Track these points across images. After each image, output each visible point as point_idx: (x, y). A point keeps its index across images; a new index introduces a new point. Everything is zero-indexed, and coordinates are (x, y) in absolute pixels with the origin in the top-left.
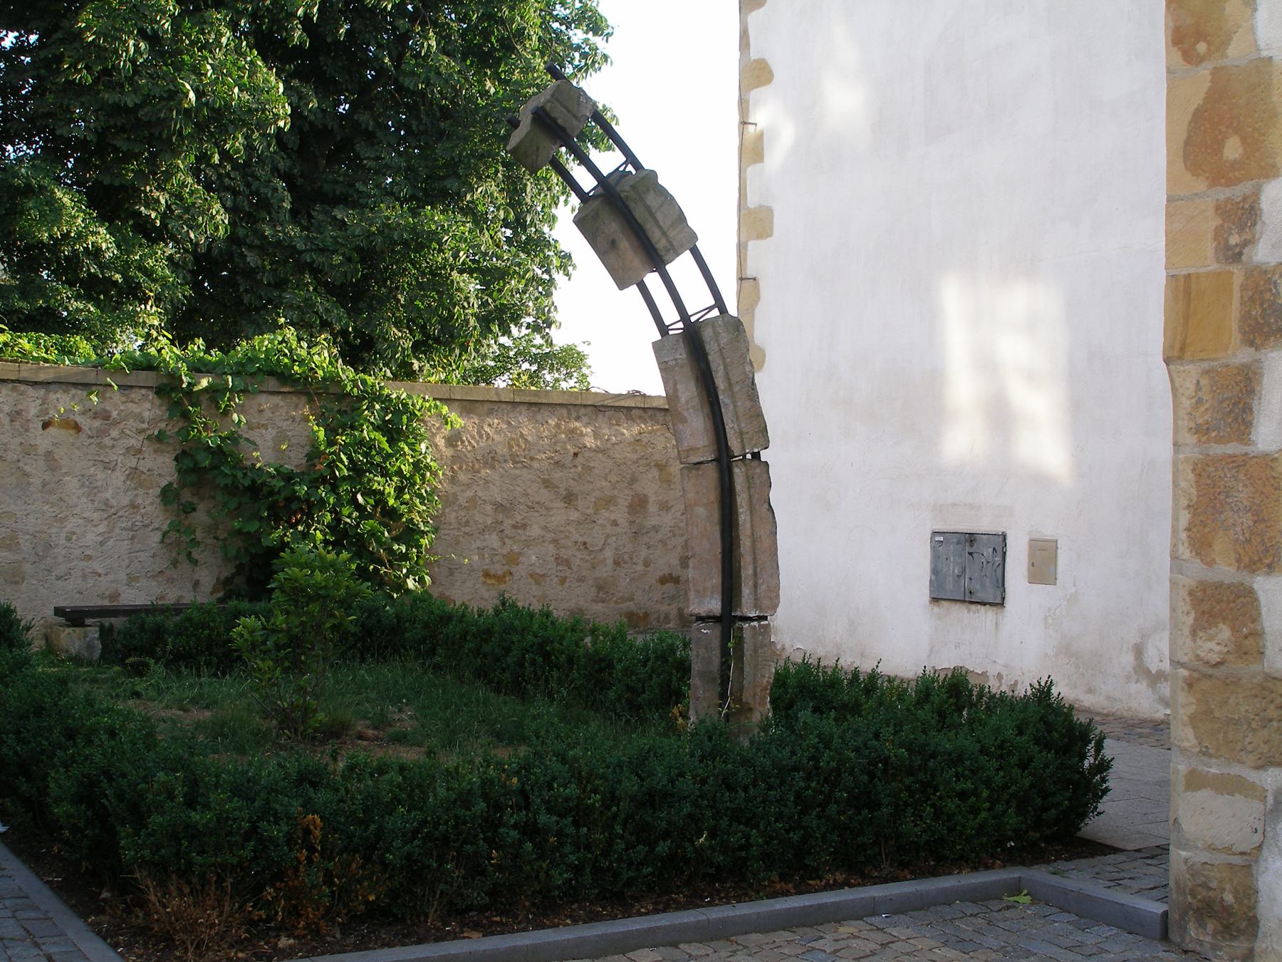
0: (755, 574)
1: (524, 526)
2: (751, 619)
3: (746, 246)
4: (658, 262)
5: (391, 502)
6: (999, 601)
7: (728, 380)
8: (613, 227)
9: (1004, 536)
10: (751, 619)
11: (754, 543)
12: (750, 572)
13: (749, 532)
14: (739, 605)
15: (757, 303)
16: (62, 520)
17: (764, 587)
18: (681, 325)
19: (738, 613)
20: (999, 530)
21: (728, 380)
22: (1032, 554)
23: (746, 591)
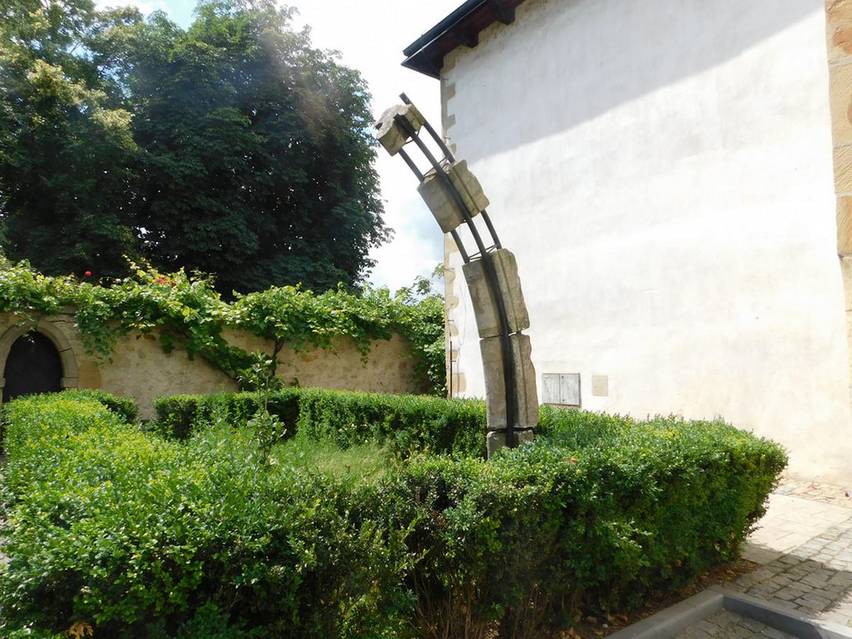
0: (526, 402)
1: (356, 377)
2: (524, 429)
3: (448, 257)
4: (466, 216)
5: (28, 529)
6: (578, 404)
7: (508, 288)
8: (441, 195)
9: (579, 374)
10: (524, 429)
11: (525, 383)
12: (523, 401)
13: (522, 377)
14: (517, 421)
15: (507, 251)
16: (146, 381)
17: (531, 410)
18: (480, 255)
19: (517, 426)
20: (577, 372)
21: (508, 288)
22: (594, 382)
23: (521, 412)
